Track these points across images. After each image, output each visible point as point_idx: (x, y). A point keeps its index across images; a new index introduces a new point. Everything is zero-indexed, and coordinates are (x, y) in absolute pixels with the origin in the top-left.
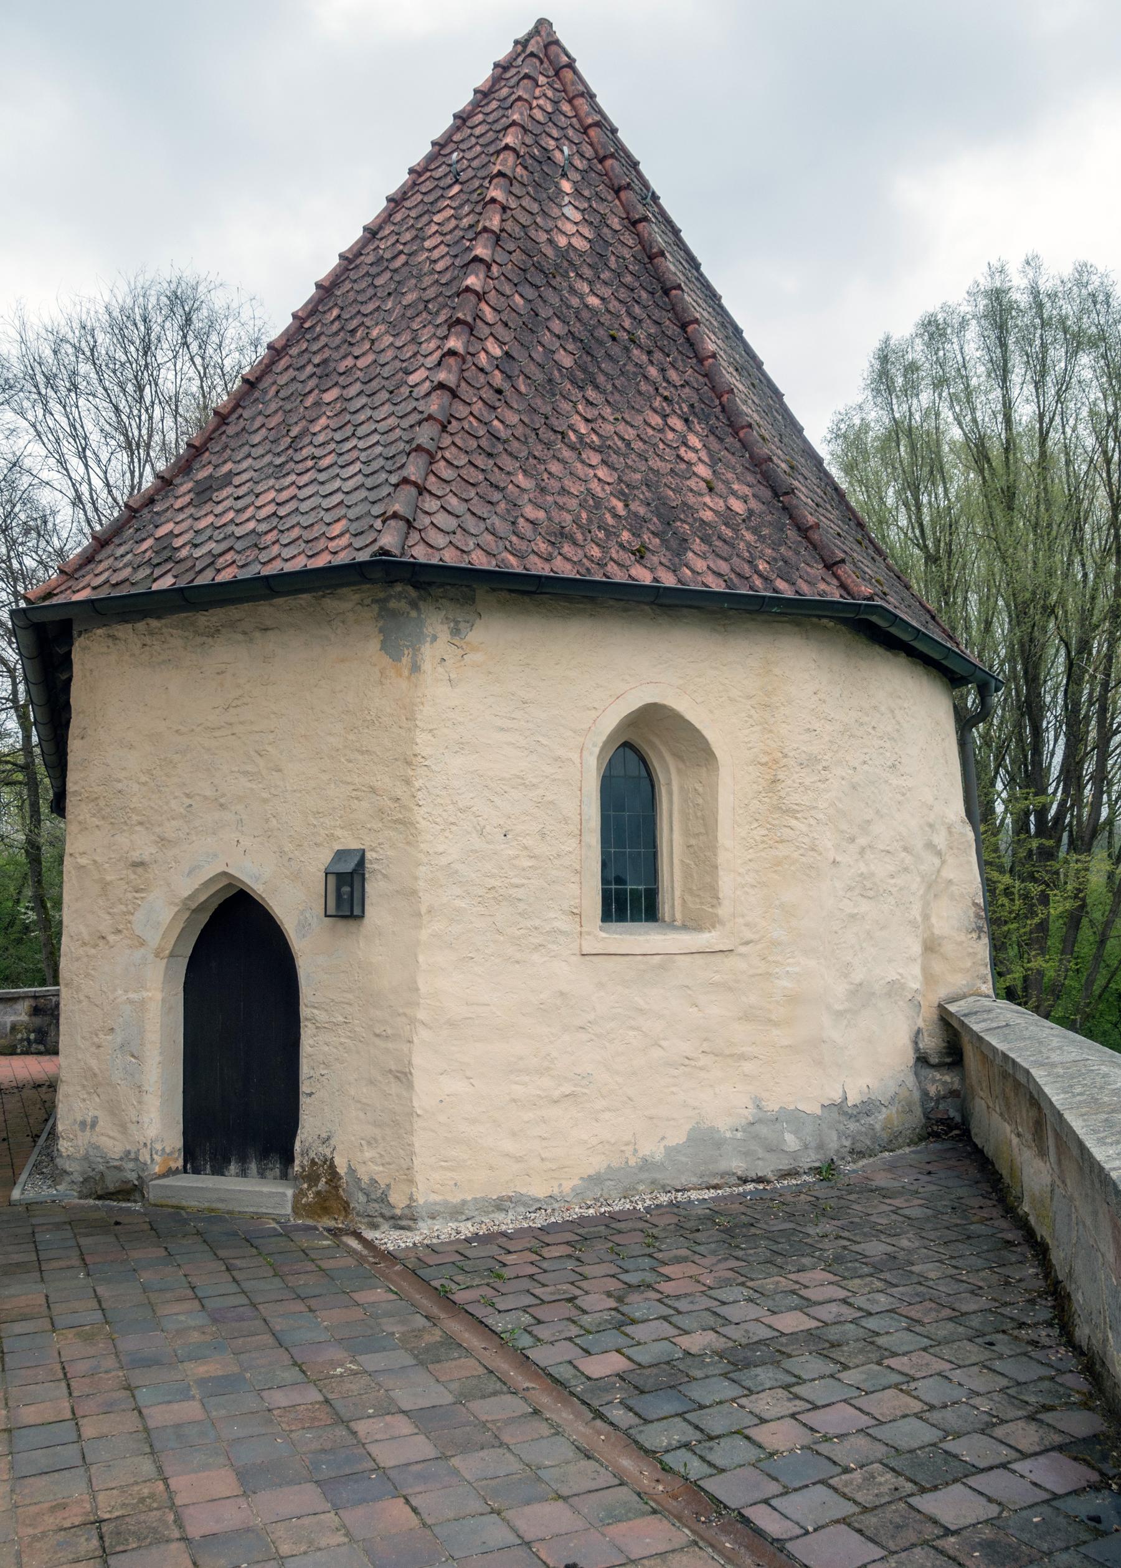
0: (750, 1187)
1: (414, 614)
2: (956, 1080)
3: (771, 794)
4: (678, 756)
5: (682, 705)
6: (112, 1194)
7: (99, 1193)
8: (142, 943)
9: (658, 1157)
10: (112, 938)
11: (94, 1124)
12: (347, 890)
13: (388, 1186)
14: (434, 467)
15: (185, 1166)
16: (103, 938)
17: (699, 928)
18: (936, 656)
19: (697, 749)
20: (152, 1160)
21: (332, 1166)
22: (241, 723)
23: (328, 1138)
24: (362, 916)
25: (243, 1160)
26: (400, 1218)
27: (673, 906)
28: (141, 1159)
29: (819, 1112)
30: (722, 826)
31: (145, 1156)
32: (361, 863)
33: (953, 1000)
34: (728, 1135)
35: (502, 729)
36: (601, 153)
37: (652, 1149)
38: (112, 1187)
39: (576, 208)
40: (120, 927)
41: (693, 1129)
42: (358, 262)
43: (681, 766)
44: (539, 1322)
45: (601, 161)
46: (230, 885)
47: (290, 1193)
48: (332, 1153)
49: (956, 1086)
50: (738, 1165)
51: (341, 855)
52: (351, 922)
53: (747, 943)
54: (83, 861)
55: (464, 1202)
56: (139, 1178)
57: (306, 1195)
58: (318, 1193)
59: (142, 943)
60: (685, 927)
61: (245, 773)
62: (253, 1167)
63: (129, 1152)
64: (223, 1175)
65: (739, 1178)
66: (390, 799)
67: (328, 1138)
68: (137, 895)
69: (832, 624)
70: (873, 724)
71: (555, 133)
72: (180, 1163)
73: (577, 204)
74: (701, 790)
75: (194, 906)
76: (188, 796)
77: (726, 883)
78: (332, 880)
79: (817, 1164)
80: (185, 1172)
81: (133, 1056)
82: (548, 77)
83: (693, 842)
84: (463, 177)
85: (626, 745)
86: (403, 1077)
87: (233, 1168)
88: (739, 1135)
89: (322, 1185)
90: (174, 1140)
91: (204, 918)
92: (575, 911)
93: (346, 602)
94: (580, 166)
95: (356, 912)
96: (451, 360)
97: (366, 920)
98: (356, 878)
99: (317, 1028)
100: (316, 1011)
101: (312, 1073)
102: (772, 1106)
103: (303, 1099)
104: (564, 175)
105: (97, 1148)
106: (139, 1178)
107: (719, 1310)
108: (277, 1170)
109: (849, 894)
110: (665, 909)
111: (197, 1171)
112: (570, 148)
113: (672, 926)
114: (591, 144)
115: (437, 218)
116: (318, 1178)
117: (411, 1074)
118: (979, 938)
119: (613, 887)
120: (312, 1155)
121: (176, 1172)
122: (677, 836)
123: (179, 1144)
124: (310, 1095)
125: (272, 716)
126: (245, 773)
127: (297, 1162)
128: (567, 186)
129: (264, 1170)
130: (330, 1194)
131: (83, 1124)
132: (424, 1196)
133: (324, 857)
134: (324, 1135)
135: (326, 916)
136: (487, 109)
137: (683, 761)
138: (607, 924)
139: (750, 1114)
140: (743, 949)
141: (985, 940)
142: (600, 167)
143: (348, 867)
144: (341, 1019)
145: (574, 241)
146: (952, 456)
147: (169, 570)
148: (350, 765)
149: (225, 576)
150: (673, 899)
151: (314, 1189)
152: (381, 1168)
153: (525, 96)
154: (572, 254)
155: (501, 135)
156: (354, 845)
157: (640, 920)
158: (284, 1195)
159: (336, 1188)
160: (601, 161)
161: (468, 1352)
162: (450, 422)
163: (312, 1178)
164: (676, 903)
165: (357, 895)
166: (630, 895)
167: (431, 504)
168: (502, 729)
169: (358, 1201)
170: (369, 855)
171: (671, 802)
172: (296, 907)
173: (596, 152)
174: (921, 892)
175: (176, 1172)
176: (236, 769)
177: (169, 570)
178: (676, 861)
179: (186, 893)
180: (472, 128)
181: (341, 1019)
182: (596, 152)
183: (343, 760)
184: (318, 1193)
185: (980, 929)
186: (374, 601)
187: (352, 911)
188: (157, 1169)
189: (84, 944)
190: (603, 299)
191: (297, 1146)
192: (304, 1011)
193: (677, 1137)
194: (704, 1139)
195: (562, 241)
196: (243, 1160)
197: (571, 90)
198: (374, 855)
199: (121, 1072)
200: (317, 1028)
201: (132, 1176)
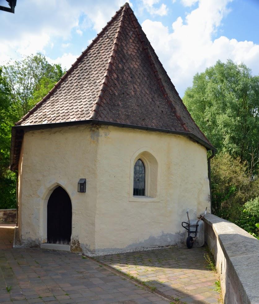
0: (161, 248)
1: (97, 131)
4: (150, 162)
5: (151, 152)
6: (33, 247)
7: (31, 246)
8: (39, 197)
9: (143, 242)
10: (32, 195)
11: (29, 233)
12: (82, 187)
13: (90, 245)
14: (102, 100)
16: (31, 195)
17: (152, 197)
19: (154, 161)
20: (41, 240)
21: (78, 242)
23: (78, 236)
24: (85, 192)
25: (60, 241)
26: (92, 251)
28: (39, 240)
29: (175, 234)
30: (157, 179)
31: (40, 239)
32: (85, 182)
33: (202, 214)
34: (157, 238)
36: (139, 34)
37: (142, 240)
38: (33, 245)
39: (133, 45)
40: (35, 193)
41: (150, 237)
45: (138, 35)
46: (58, 185)
47: (70, 247)
50: (158, 244)
51: (81, 180)
52: (83, 193)
54: (26, 180)
55: (105, 249)
56: (39, 243)
58: (76, 247)
59: (39, 197)
60: (150, 197)
62: (62, 242)
63: (36, 239)
64: (55, 243)
65: (159, 246)
67: (78, 236)
71: (129, 29)
72: (47, 241)
75: (50, 189)
76: (49, 167)
77: (159, 188)
79: (174, 244)
80: (48, 243)
81: (37, 219)
82: (127, 16)
85: (139, 159)
86: (93, 224)
87: (58, 242)
88: (159, 238)
89: (76, 245)
90: (46, 237)
91: (52, 192)
93: (82, 128)
94: (134, 36)
95: (84, 191)
97: (86, 193)
98: (85, 184)
101: (74, 223)
102: (166, 233)
103: (72, 228)
104: (131, 38)
105: (30, 238)
106: (39, 243)
110: (146, 193)
111: (50, 243)
113: (147, 197)
116: (75, 244)
117: (94, 223)
118: (209, 202)
120: (74, 239)
121: (46, 243)
122: (149, 179)
123: (46, 237)
124: (74, 228)
127: (71, 241)
128: (131, 41)
130: (78, 247)
131: (27, 233)
132: (97, 248)
133: (77, 180)
134: (77, 235)
138: (134, 196)
139: (161, 234)
140: (161, 202)
141: (210, 202)
142: (138, 36)
143: (83, 182)
144: (81, 213)
145: (132, 53)
146: (253, 92)
147: (46, 120)
149: (58, 122)
151: (75, 246)
152: (88, 242)
154: (132, 56)
156: (84, 178)
158: (69, 247)
159: (79, 246)
160: (138, 35)
161: (108, 271)
162: (105, 91)
163: (74, 244)
165: (84, 187)
167: (102, 109)
169: (84, 249)
171: (148, 170)
175: (46, 243)
177: (46, 120)
179: (48, 187)
181: (81, 213)
184: (76, 247)
185: (209, 200)
186: (89, 128)
187: (83, 191)
188: (42, 242)
189: (27, 197)
190: (138, 66)
191: (71, 238)
192: (73, 211)
193: (147, 238)
194: (152, 239)
195: (129, 53)
196: (60, 241)
197: (133, 19)
198: (88, 180)
199: (34, 221)
201: (38, 243)
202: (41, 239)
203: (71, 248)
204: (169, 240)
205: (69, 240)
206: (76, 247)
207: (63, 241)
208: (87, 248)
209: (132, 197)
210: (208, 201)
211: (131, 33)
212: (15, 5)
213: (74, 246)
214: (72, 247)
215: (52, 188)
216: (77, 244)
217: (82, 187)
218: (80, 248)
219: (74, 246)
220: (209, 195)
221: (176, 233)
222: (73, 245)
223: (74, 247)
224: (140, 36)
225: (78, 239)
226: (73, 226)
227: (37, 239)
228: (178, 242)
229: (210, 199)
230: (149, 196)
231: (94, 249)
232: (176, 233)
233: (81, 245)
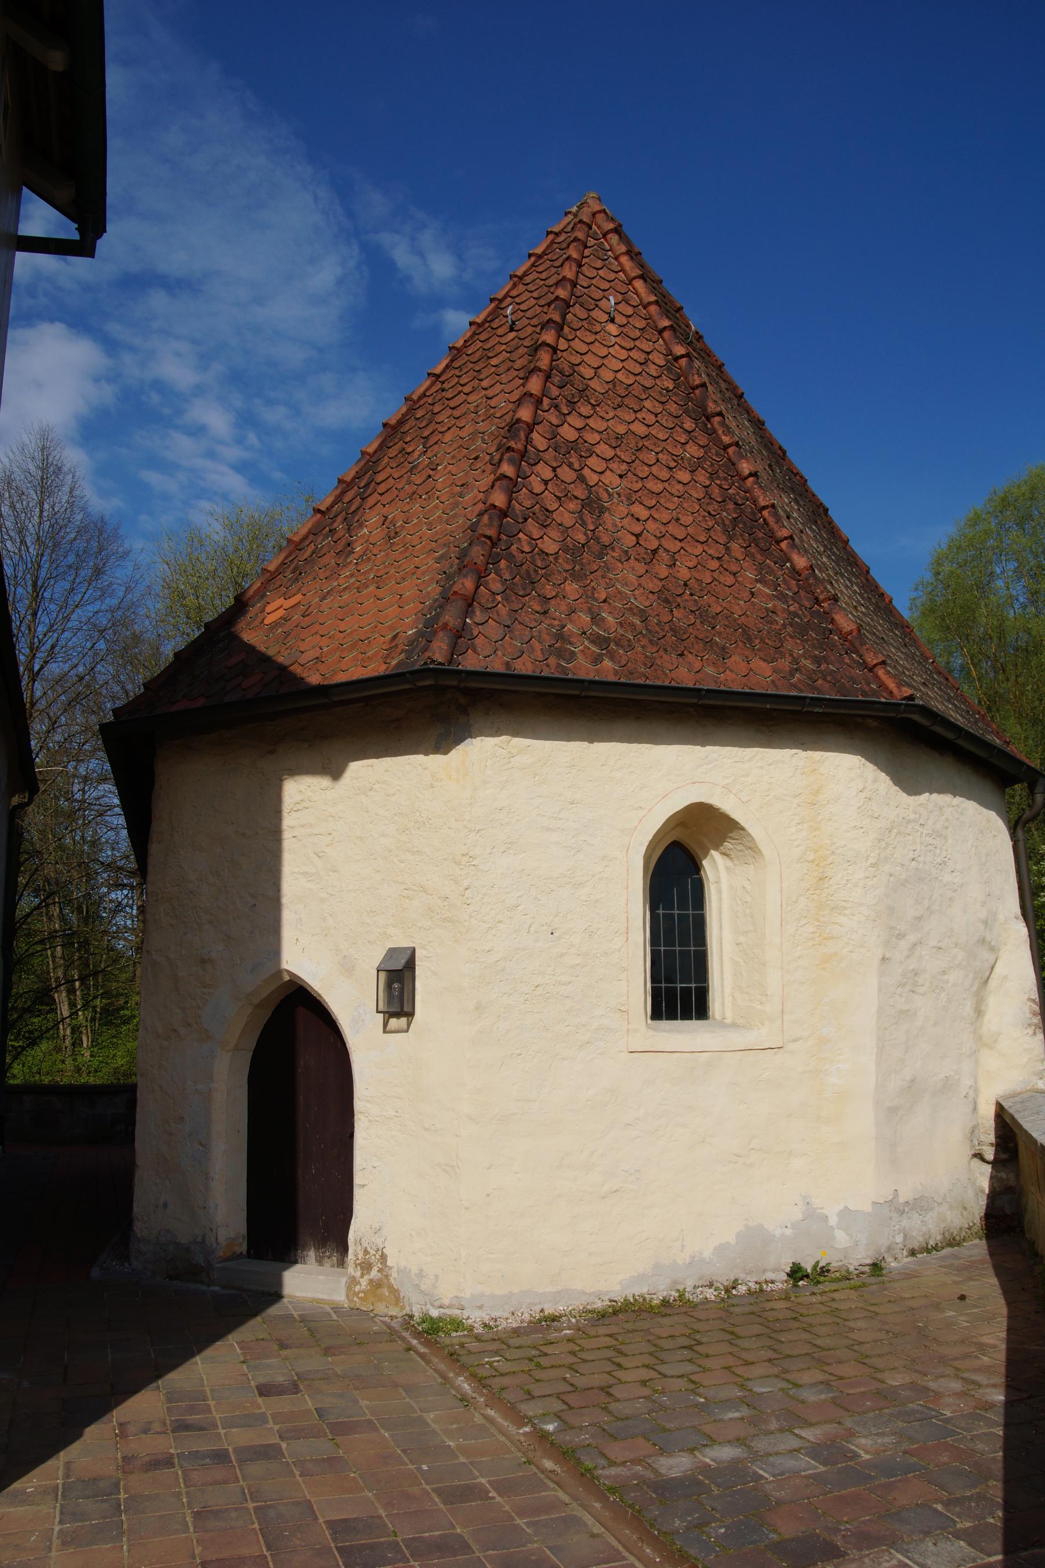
2: (1012, 1176)
3: (818, 892)
11: (165, 1205)
13: (437, 1276)
15: (248, 1251)
18: (982, 754)
21: (384, 1258)
22: (302, 826)
27: (723, 1004)
32: (410, 965)
34: (778, 1232)
35: (548, 829)
42: (422, 402)
43: (729, 863)
44: (609, 1373)
48: (383, 1243)
49: (1012, 1182)
51: (392, 952)
53: (795, 1040)
57: (359, 1283)
60: (734, 1025)
61: (305, 874)
66: (440, 898)
68: (206, 991)
69: (875, 724)
70: (921, 821)
72: (244, 1248)
73: (623, 344)
74: (749, 887)
75: (256, 1001)
78: (383, 976)
81: (201, 1144)
83: (742, 939)
84: (518, 325)
88: (788, 1232)
89: (374, 1273)
91: (266, 1014)
92: (622, 1008)
96: (505, 482)
98: (407, 974)
99: (370, 1121)
100: (368, 1105)
107: (773, 1335)
108: (335, 1259)
109: (899, 990)
112: (615, 297)
113: (722, 1025)
114: (636, 294)
115: (494, 362)
118: (1035, 1033)
119: (693, 985)
120: (365, 1244)
123: (244, 1230)
124: (363, 1186)
125: (331, 819)
126: (305, 874)
127: (351, 1251)
129: (322, 1258)
133: (377, 956)
134: (377, 1226)
135: (378, 1012)
136: (540, 269)
137: (731, 859)
143: (399, 964)
148: (403, 865)
150: (723, 997)
153: (575, 256)
155: (552, 290)
157: (675, 1018)
159: (387, 1276)
164: (726, 1001)
166: (679, 987)
168: (548, 829)
170: (418, 954)
171: (720, 900)
172: (351, 1002)
173: (641, 299)
174: (975, 988)
176: (296, 870)
178: (726, 959)
180: (527, 284)
182: (641, 299)
183: (395, 860)
184: (371, 1281)
192: (358, 1105)
200: (370, 1121)
202: (213, 1240)
203: (349, 1288)
204: (842, 1239)
205: (343, 1248)
206: (376, 1285)
207: (317, 1249)
208: (423, 1287)
209: (643, 1028)
210: (1030, 1031)
211: (611, 298)
212: (100, 229)
213: (362, 1276)
214: (353, 1281)
215: (265, 993)
216: (376, 1269)
217: (72, 997)
218: (390, 1287)
219: (362, 1276)
220: (1033, 1001)
221: (874, 1203)
222: (358, 1274)
223: (364, 1282)
224: (731, 450)
225: (379, 1242)
226: (358, 1179)
227: (199, 1239)
228: (889, 1249)
229: (1037, 1020)
230: (728, 1021)
231: (457, 1297)
232: (874, 1203)
233: (394, 1274)
